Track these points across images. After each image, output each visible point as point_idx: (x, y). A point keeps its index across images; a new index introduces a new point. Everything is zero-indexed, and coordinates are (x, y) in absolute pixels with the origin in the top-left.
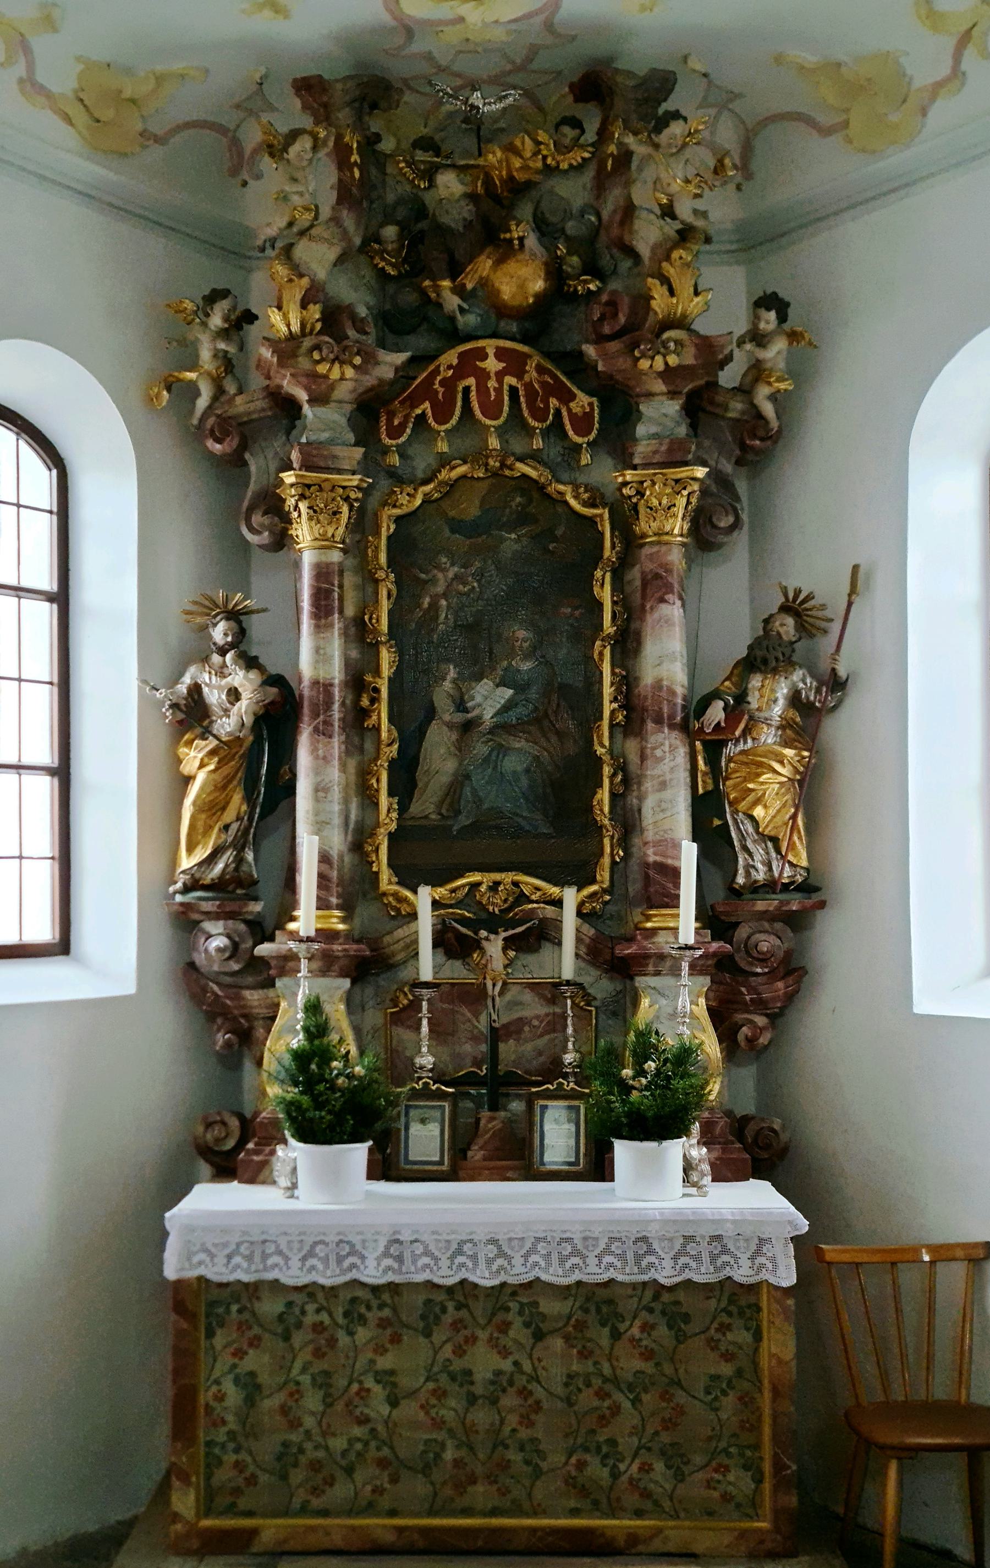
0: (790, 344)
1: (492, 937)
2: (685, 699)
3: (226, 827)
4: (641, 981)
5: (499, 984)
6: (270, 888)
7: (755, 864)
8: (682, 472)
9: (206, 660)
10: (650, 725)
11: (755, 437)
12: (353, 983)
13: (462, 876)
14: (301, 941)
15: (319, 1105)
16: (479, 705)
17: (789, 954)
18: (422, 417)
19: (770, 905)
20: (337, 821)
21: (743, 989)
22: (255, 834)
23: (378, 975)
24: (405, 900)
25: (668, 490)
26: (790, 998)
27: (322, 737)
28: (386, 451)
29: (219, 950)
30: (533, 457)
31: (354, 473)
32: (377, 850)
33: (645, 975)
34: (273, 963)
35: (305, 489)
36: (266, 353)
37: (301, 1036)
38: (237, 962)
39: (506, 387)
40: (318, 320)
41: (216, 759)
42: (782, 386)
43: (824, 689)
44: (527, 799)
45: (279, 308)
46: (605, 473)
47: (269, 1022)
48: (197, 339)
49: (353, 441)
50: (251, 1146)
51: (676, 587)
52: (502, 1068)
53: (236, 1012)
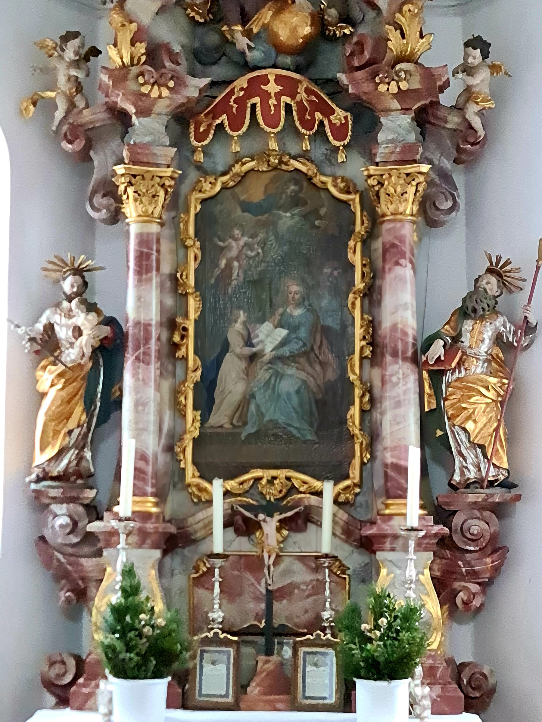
0: (492, 74)
1: (268, 519)
2: (415, 339)
3: (70, 432)
4: (380, 555)
5: (273, 557)
6: (103, 477)
7: (468, 465)
8: (411, 169)
9: (58, 305)
10: (388, 358)
11: (467, 142)
12: (165, 553)
13: (247, 472)
14: (120, 520)
15: (129, 650)
16: (262, 341)
17: (494, 538)
18: (221, 126)
19: (478, 498)
20: (152, 428)
21: (460, 563)
22: (92, 438)
23: (183, 547)
24: (205, 490)
25: (402, 181)
26: (497, 570)
27: (141, 364)
28: (194, 150)
29: (61, 526)
30: (305, 156)
31: (168, 166)
32: (184, 451)
33: (383, 550)
34: (101, 537)
35: (133, 179)
36: (105, 78)
37: (119, 594)
38: (76, 536)
39: (282, 104)
40: (143, 55)
41: (63, 380)
42: (487, 105)
43: (519, 331)
44: (296, 412)
45: (115, 45)
46: (355, 167)
47: (99, 582)
48: (55, 68)
49: (168, 144)
50: (81, 680)
51: (408, 255)
52: (276, 623)
53: (76, 575)
